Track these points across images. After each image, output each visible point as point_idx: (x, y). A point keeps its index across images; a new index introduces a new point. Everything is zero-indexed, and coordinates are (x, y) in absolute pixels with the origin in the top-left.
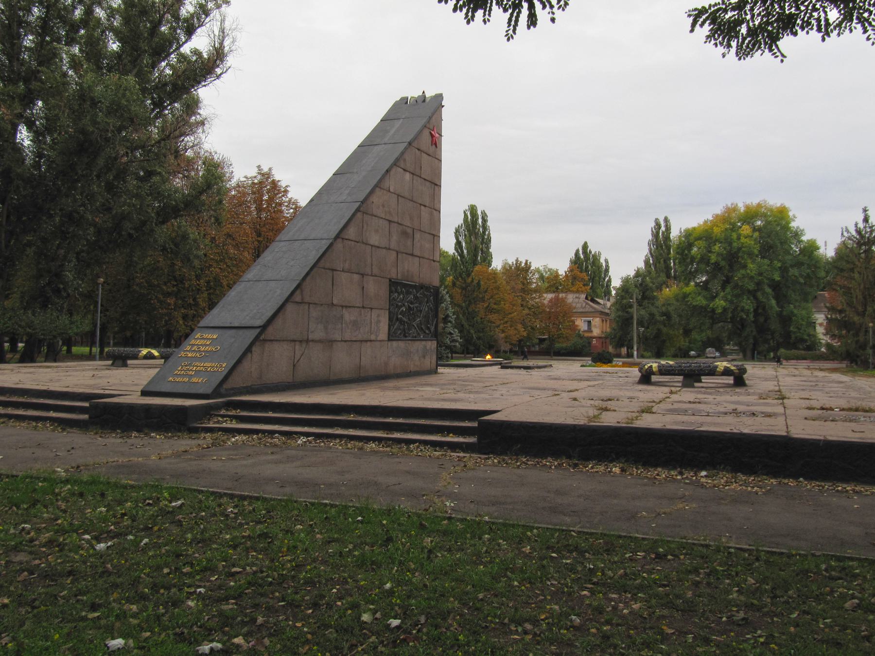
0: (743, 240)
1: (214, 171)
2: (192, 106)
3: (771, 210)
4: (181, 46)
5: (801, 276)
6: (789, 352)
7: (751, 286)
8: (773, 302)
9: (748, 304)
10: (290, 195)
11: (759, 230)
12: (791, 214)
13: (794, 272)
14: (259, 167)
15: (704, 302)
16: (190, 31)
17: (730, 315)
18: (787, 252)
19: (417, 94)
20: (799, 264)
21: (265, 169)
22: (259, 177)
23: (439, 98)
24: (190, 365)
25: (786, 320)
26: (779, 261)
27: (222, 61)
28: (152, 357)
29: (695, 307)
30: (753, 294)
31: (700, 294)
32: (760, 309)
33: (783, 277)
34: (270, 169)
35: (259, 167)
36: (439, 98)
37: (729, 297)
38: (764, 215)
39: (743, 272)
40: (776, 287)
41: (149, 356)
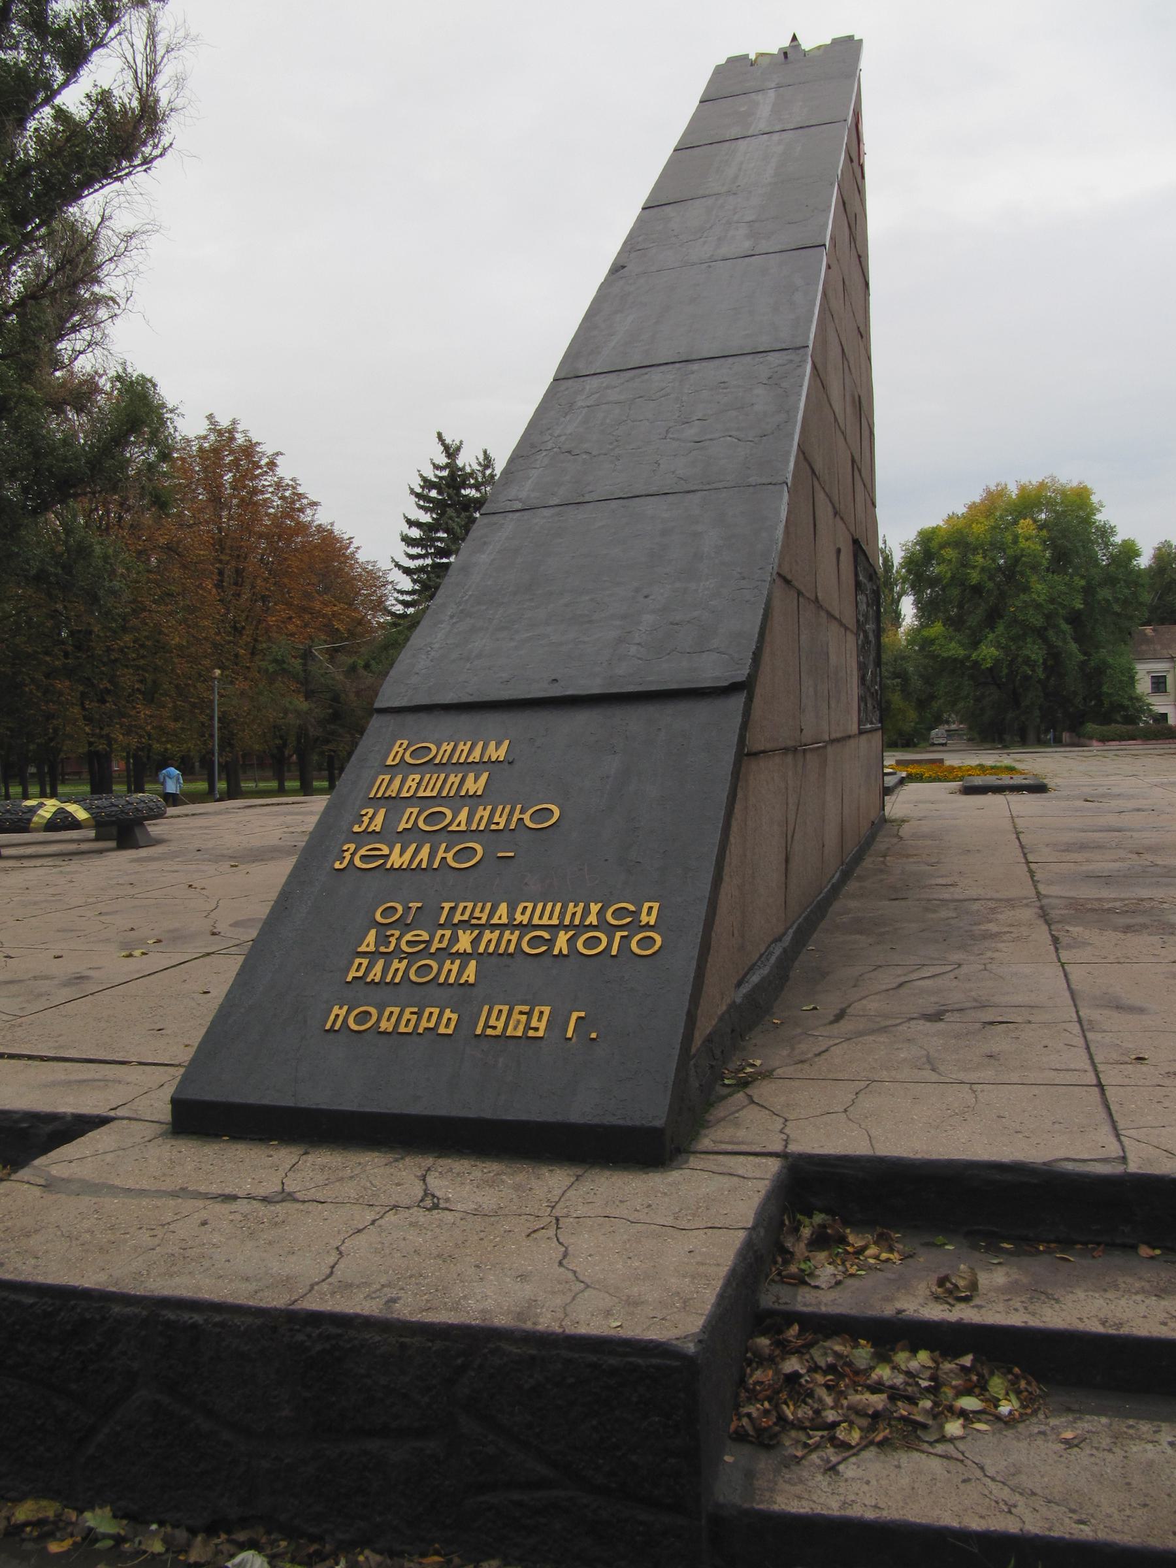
0: (1023, 544)
1: (139, 407)
2: (79, 262)
3: (1063, 493)
4: (57, 92)
5: (1117, 600)
6: (1105, 728)
7: (1038, 621)
8: (1073, 647)
9: (1034, 651)
10: (280, 471)
11: (1042, 526)
12: (1094, 499)
13: (1105, 593)
14: (210, 417)
15: (961, 652)
16: (75, 58)
17: (1005, 671)
18: (1095, 561)
19: (775, 44)
20: (1110, 580)
21: (224, 422)
22: (212, 437)
23: (847, 50)
24: (427, 917)
25: (1094, 675)
26: (1083, 577)
27: (152, 132)
28: (69, 823)
29: (945, 660)
30: (1041, 633)
31: (951, 639)
32: (1055, 658)
33: (1086, 603)
34: (234, 422)
35: (210, 417)
36: (847, 50)
37: (1003, 641)
38: (1050, 504)
39: (1024, 597)
40: (1075, 619)
41: (62, 822)
